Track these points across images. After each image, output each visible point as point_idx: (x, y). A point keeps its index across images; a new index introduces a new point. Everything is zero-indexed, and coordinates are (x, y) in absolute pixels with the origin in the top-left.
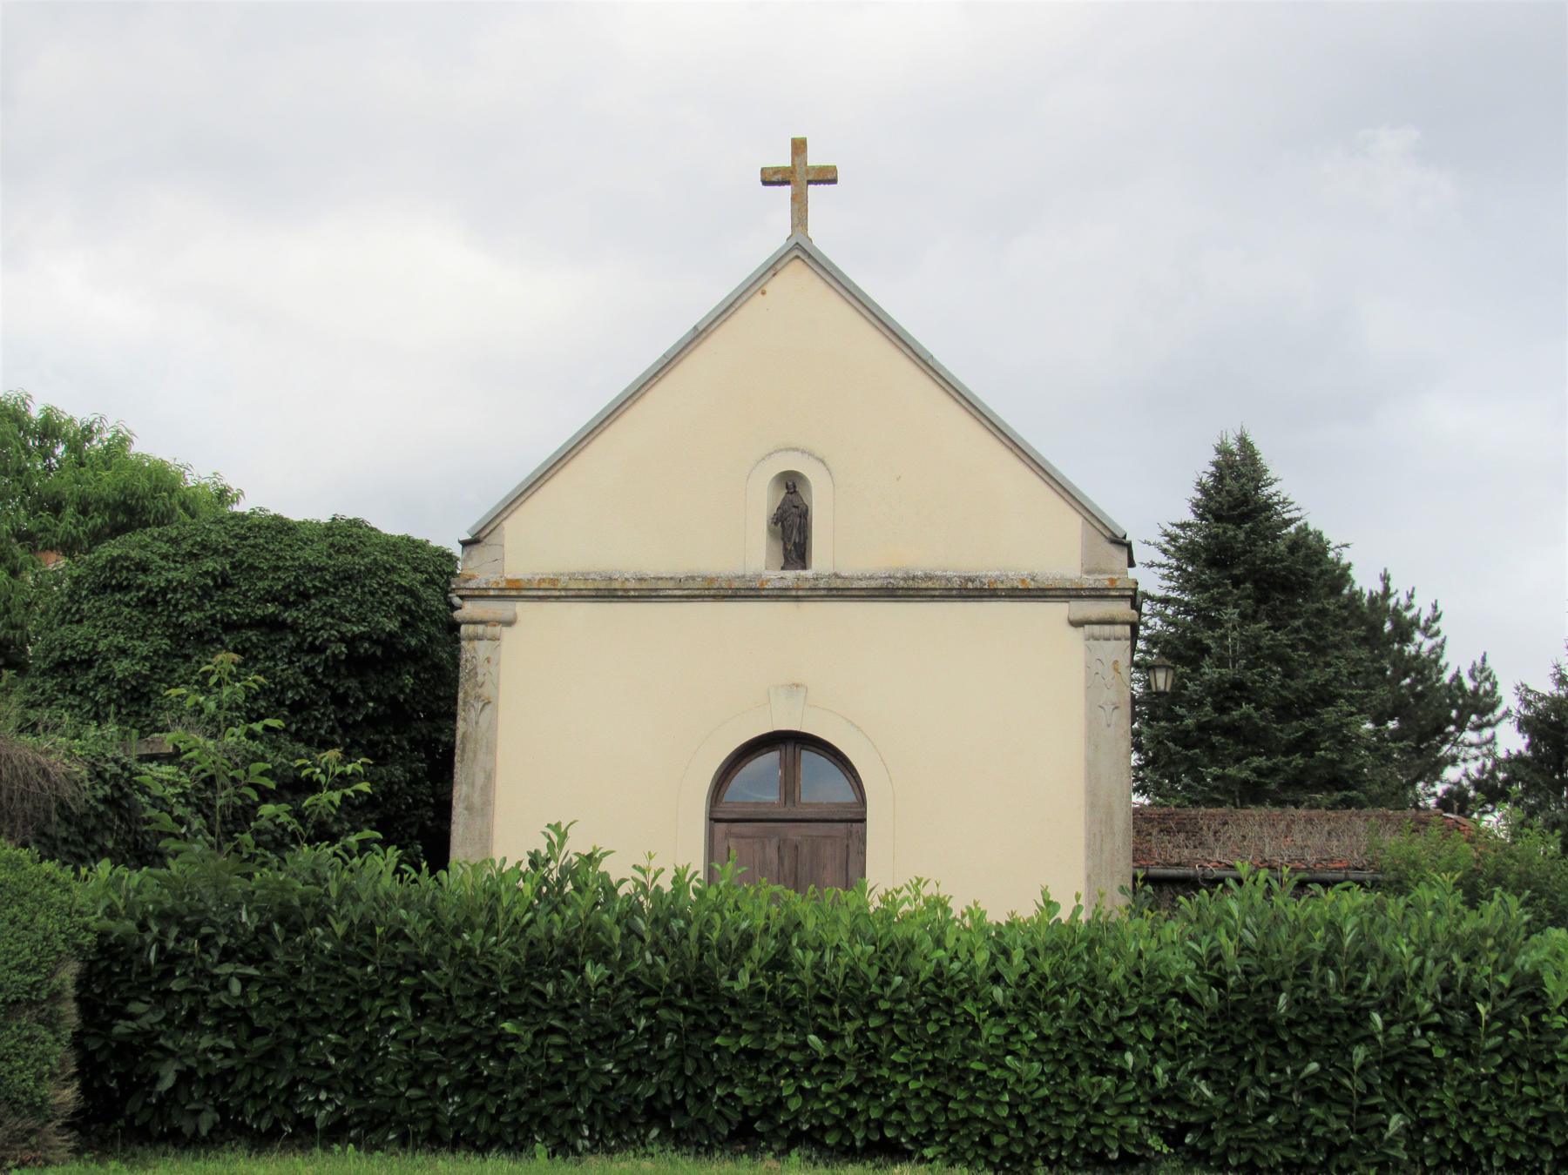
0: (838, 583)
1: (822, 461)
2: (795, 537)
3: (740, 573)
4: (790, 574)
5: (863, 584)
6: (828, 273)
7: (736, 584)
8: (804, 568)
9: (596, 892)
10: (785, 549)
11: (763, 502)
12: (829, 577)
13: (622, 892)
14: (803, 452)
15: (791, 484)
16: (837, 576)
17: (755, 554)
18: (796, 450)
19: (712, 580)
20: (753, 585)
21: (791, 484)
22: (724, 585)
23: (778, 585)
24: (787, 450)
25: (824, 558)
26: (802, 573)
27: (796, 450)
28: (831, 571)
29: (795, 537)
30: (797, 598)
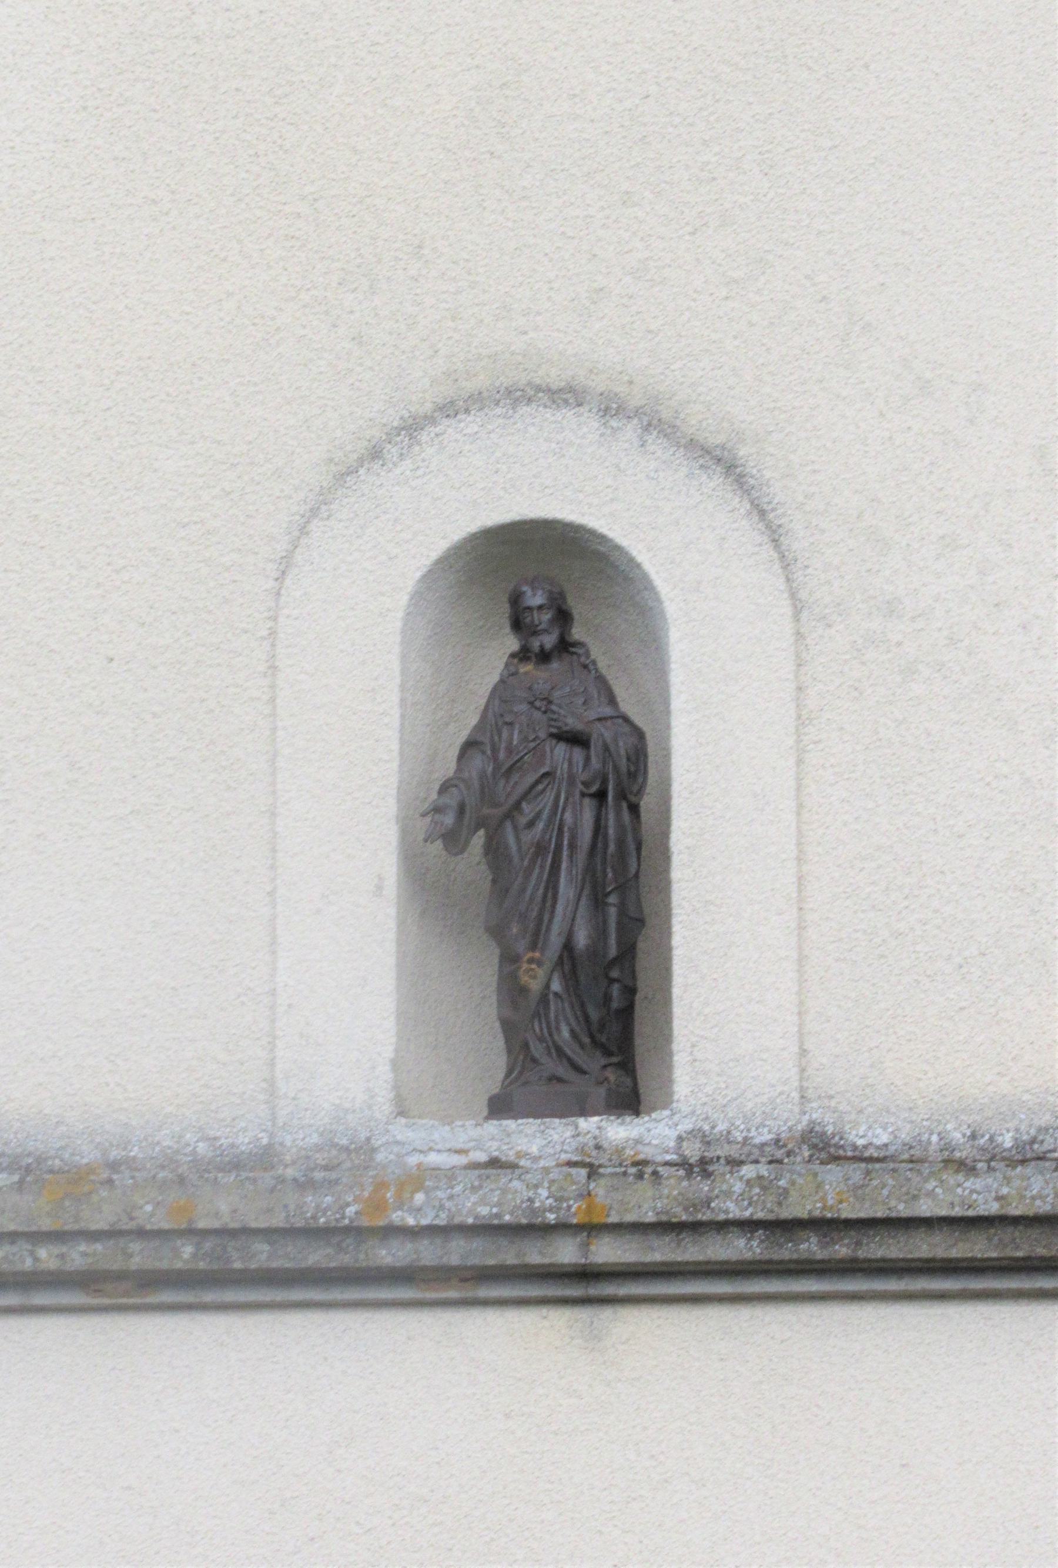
0: (831, 1192)
1: (724, 463)
2: (571, 919)
3: (245, 1139)
4: (542, 1141)
5: (981, 1194)
6: (151, 1281)
7: (221, 1207)
8: (629, 1101)
9: (1021, 1121)
10: (511, 989)
11: (349, 725)
12: (778, 1153)
13: (380, 1157)
14: (612, 409)
15: (545, 607)
16: (824, 1147)
17: (315, 1002)
18: (566, 396)
19: (75, 1180)
20: (318, 1206)
21: (545, 607)
22: (150, 1212)
23: (476, 1204)
24: (520, 395)
25: (766, 1012)
26: (618, 1131)
27: (566, 396)
28: (788, 1119)
29: (571, 919)
30: (586, 1286)
